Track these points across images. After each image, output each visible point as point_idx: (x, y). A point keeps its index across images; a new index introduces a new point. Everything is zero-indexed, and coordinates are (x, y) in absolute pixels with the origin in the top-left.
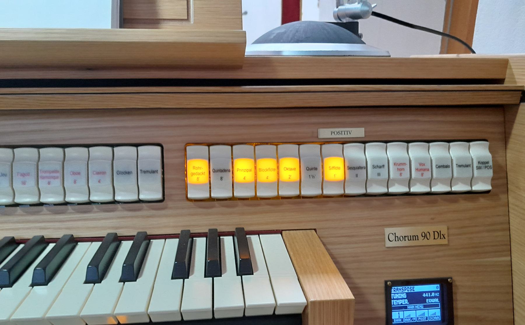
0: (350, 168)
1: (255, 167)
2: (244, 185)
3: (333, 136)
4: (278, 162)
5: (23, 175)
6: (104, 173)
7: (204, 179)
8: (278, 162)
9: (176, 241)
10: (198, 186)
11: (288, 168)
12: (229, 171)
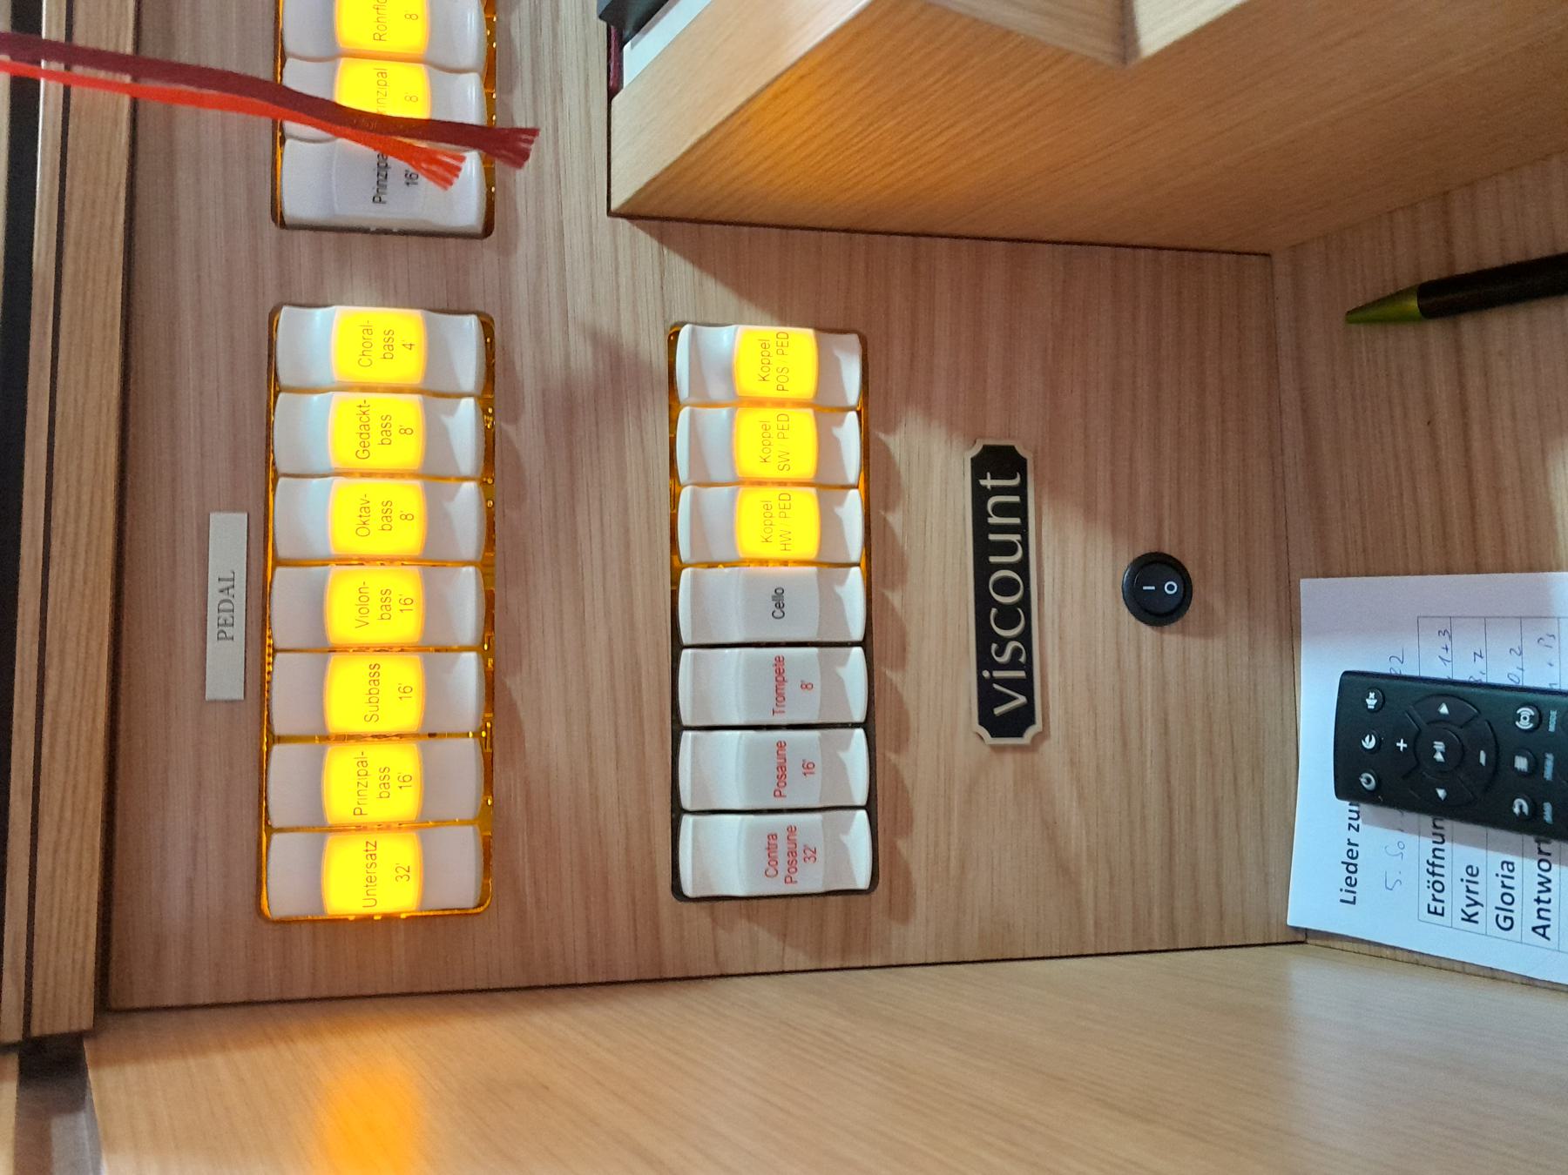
1: (360, 828)
3: (238, 631)
4: (343, 649)
8: (343, 649)
11: (359, 521)
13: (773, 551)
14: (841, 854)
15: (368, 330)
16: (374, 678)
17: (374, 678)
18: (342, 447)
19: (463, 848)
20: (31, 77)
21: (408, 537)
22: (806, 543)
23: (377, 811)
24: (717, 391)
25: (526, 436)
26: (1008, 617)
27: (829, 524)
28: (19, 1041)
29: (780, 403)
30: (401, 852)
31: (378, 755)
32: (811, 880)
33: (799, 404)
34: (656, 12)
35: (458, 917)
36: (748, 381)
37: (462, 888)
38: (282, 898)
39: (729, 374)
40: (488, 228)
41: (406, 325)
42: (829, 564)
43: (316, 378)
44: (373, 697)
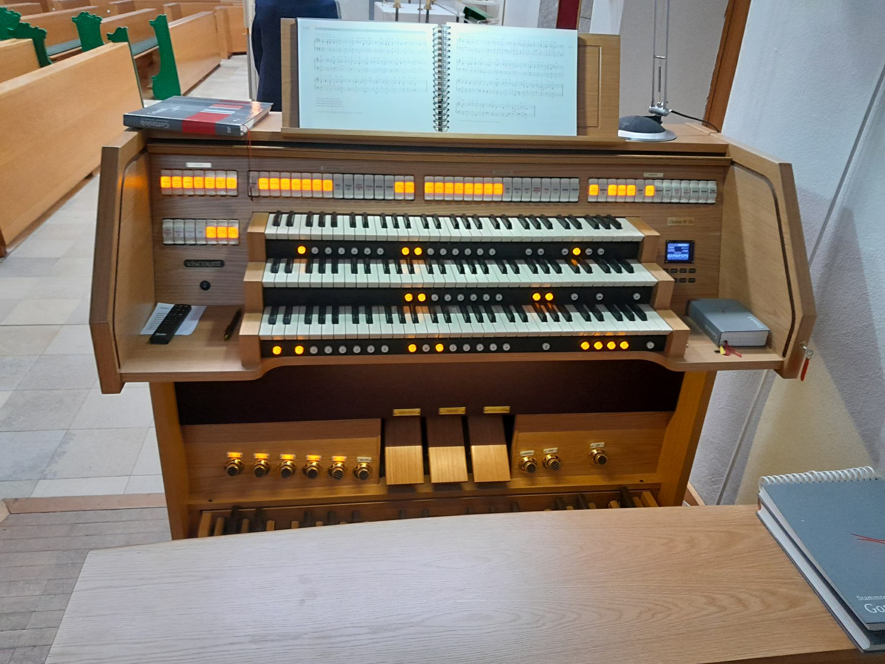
0: (392, 187)
2: (400, 194)
5: (527, 189)
6: (350, 186)
7: (330, 189)
9: (305, 216)
10: (593, 197)
12: (361, 187)
13: (208, 231)
14: (168, 240)
15: (233, 182)
16: (265, 184)
17: (265, 184)
18: (218, 178)
19: (169, 193)
20: (34, 44)
21: (207, 186)
22: (209, 236)
23: (173, 183)
24: (230, 225)
25: (223, 200)
26: (200, 264)
27: (212, 239)
28: (341, 306)
29: (171, 182)
30: (168, 185)
31: (180, 182)
32: (165, 236)
33: (171, 179)
34: (166, 139)
35: (160, 192)
36: (230, 229)
37: (164, 192)
38: (164, 172)
39: (232, 226)
40: (252, 197)
41: (234, 186)
42: (207, 239)
43: (228, 176)
44: (187, 182)
